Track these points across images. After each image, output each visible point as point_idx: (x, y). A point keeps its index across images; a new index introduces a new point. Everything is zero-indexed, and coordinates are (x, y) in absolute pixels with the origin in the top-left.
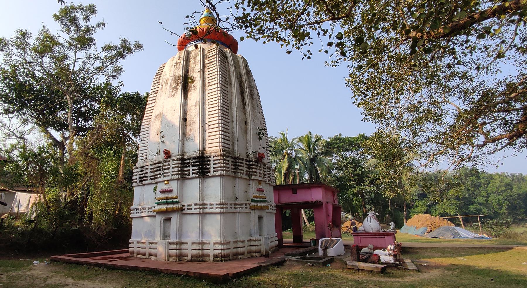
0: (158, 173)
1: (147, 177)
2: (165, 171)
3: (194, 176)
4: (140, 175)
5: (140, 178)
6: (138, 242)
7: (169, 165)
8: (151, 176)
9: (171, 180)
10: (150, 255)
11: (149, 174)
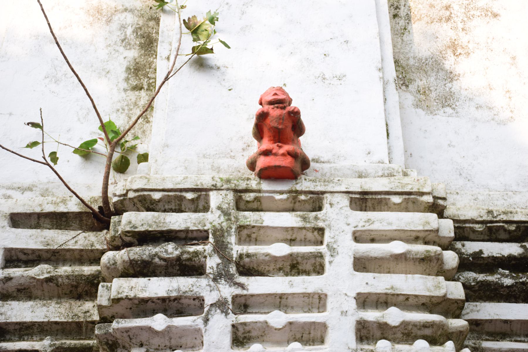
0: (158, 287)
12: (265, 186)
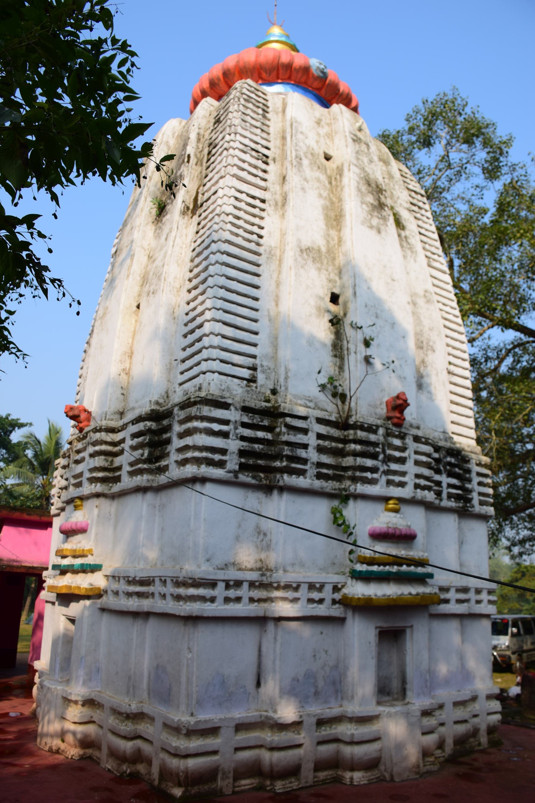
0: (369, 463)
1: (305, 461)
2: (394, 467)
3: (452, 504)
4: (243, 438)
5: (242, 453)
6: (240, 727)
7: (403, 449)
8: (319, 465)
9: (413, 502)
10: (335, 763)
11: (312, 455)
12: (394, 428)
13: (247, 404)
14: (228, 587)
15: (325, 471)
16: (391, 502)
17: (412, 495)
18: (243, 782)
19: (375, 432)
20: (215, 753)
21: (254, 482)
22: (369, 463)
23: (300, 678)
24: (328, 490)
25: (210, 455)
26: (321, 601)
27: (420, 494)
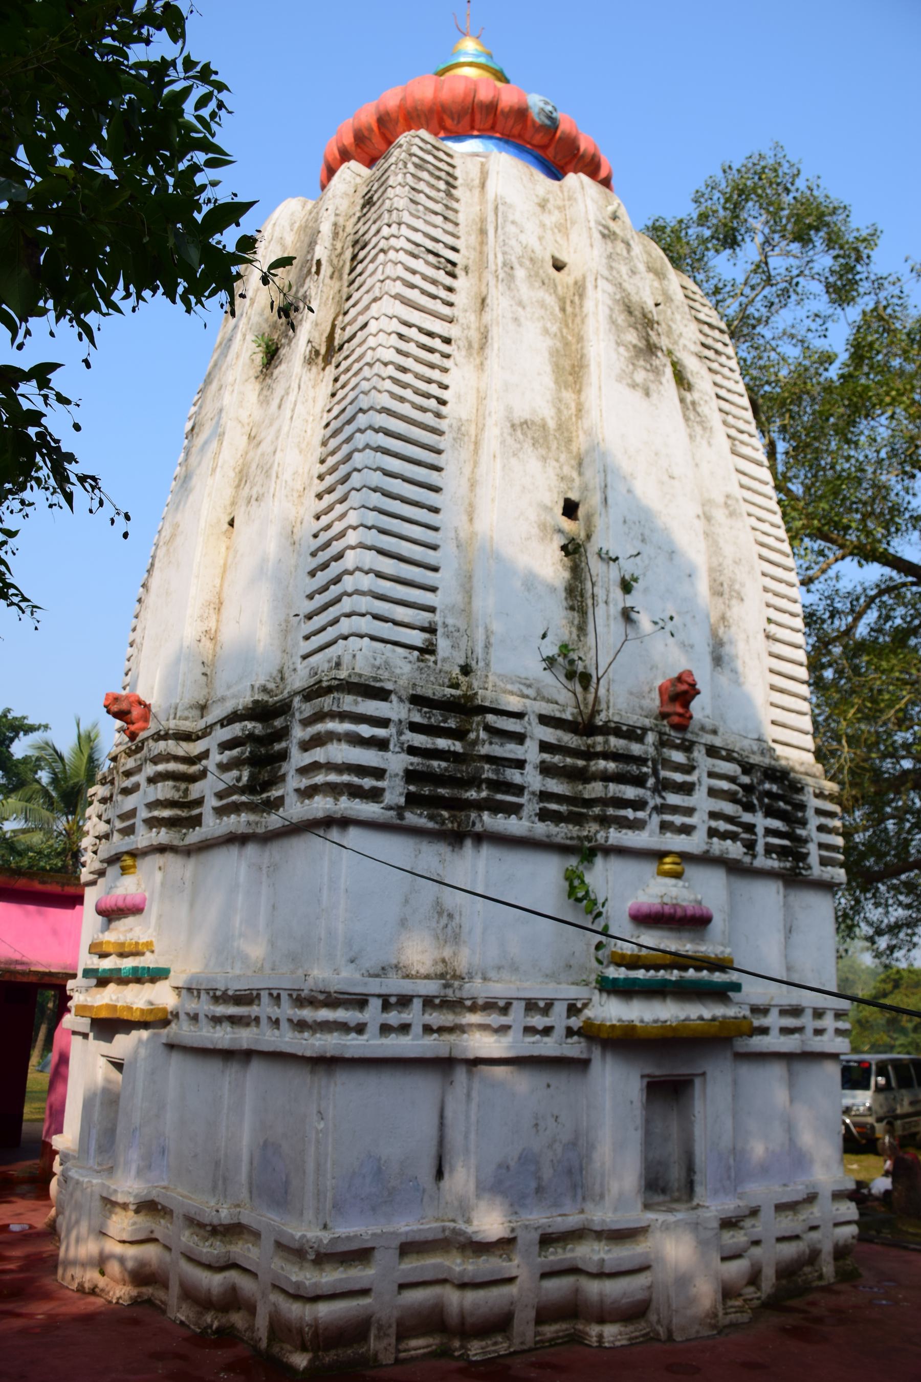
0: (630, 792)
1: (519, 790)
2: (673, 799)
4: (412, 750)
5: (410, 776)
8: (545, 796)
9: (706, 859)
10: (572, 1310)
11: (532, 779)
12: (673, 733)
13: (419, 691)
14: (386, 1006)
15: (554, 806)
16: (668, 860)
17: (704, 847)
18: (414, 1343)
19: (640, 739)
20: (365, 1292)
21: (431, 825)
22: (630, 792)
23: (512, 1164)
24: (559, 840)
25: (355, 780)
26: (547, 1031)
27: (718, 846)
